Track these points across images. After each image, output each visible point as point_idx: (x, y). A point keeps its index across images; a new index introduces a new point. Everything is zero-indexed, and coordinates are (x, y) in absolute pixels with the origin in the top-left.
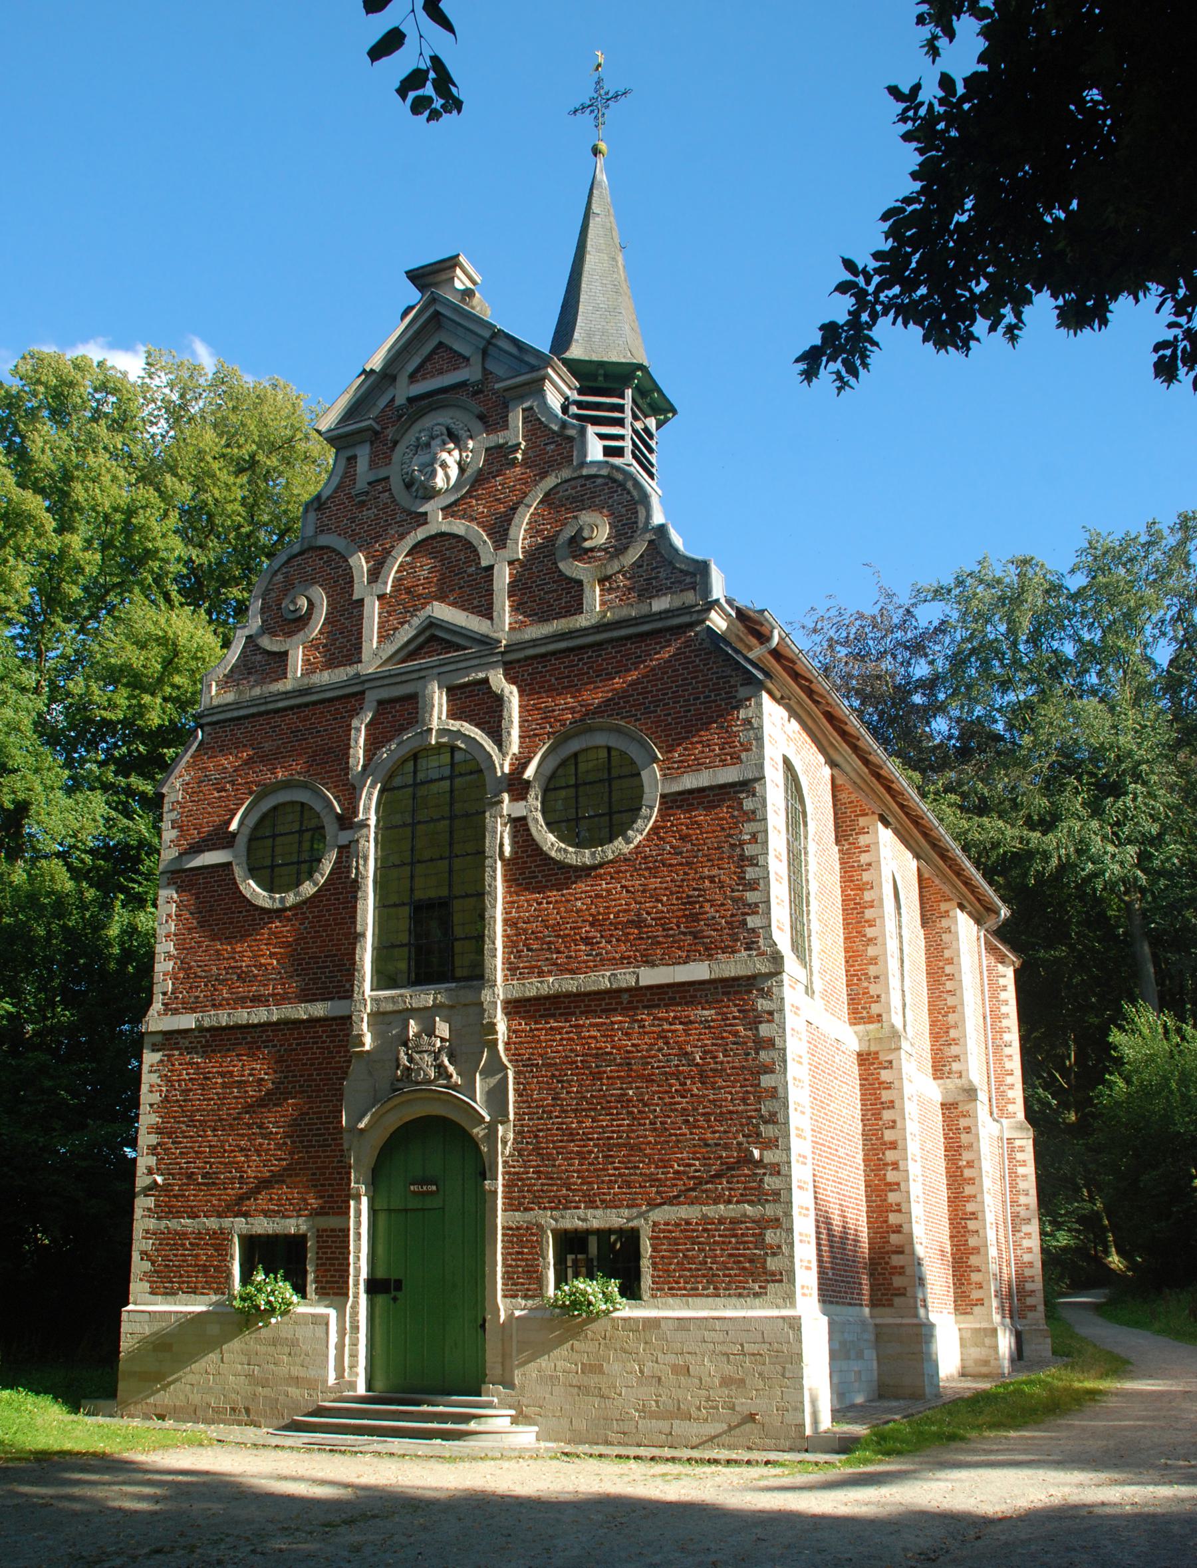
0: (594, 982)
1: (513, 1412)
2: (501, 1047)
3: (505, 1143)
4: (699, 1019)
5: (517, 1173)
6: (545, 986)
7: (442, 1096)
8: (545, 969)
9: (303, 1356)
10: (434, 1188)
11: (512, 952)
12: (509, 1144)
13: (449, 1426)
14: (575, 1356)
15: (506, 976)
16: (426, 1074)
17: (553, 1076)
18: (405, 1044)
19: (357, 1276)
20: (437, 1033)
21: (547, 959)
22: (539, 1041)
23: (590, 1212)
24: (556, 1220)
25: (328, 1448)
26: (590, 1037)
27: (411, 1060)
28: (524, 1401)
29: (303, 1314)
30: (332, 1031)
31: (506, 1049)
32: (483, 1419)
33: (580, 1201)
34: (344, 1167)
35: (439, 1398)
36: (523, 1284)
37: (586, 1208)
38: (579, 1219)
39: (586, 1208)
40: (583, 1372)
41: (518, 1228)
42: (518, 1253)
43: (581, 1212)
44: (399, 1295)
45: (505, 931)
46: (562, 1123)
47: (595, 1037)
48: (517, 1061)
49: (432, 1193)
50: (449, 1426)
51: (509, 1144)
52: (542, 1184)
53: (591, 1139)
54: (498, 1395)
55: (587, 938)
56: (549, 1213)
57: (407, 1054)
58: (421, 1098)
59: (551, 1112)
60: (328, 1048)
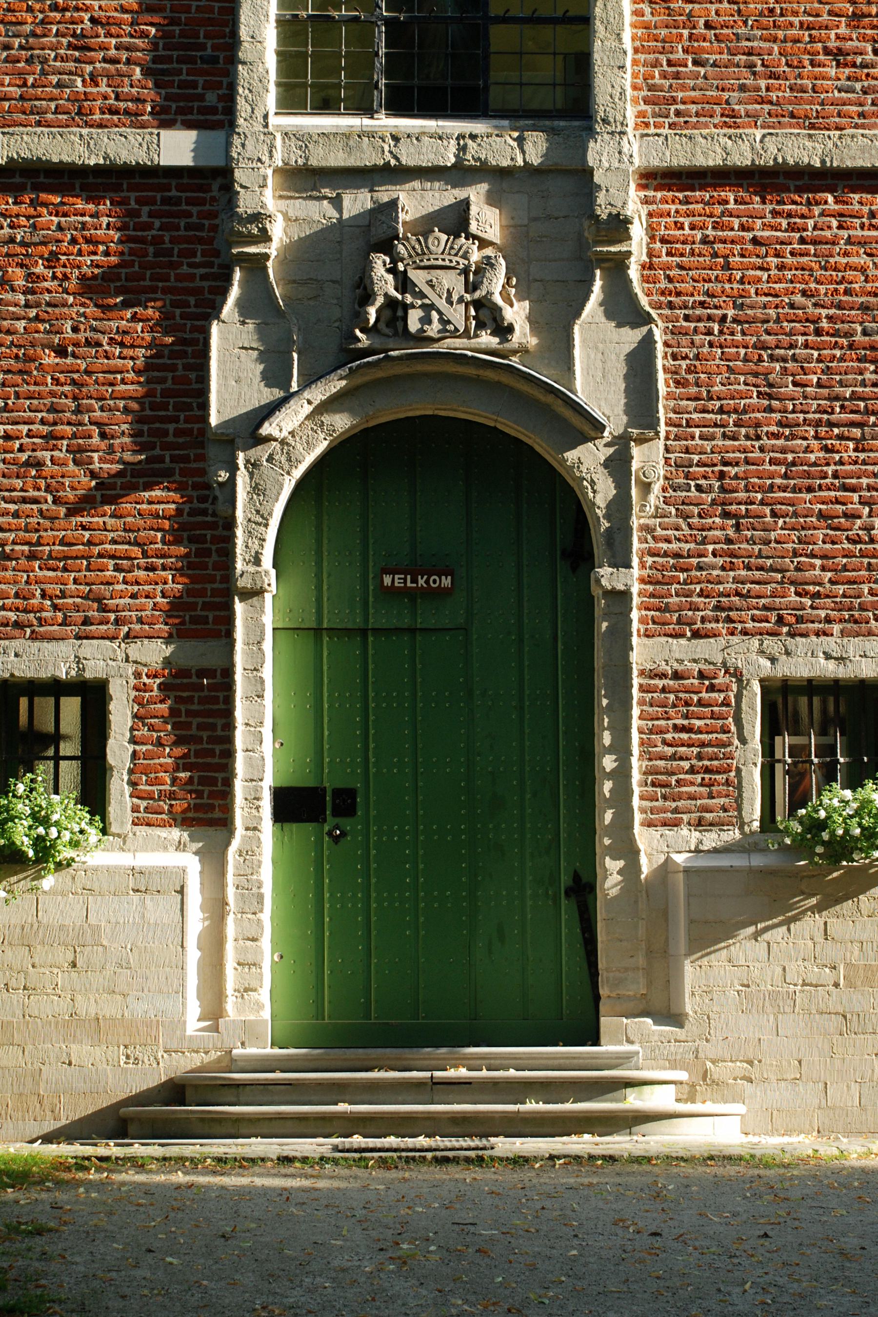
0: (863, 150)
1: (682, 1075)
2: (634, 273)
3: (646, 488)
4: (599, 364)
5: (677, 555)
6: (745, 147)
7: (489, 374)
8: (740, 108)
9: (110, 968)
10: (446, 582)
11: (656, 64)
12: (656, 488)
13: (532, 1106)
14: (831, 952)
15: (641, 114)
16: (444, 322)
17: (762, 346)
18: (387, 246)
19: (254, 780)
20: (473, 228)
21: (743, 88)
22: (727, 267)
23: (854, 645)
24: (773, 660)
25: (429, 1155)
26: (848, 267)
27: (404, 283)
28: (708, 1050)
29: (110, 871)
30: (166, 201)
31: (645, 279)
32: (646, 1088)
33: (828, 620)
34: (213, 526)
35: (408, 1053)
36: (692, 797)
37: (843, 633)
38: (828, 656)
39: (843, 633)
40: (850, 984)
41: (677, 676)
42: (677, 728)
43: (831, 644)
44: (347, 824)
45: (637, 13)
46: (784, 451)
47: (863, 270)
48: (671, 306)
49: (442, 592)
50: (532, 1106)
51: (656, 488)
52: (736, 580)
53: (854, 489)
54: (644, 1039)
55: (840, 51)
56: (755, 642)
57: (392, 271)
58: (426, 375)
59: (758, 425)
60: (157, 241)
